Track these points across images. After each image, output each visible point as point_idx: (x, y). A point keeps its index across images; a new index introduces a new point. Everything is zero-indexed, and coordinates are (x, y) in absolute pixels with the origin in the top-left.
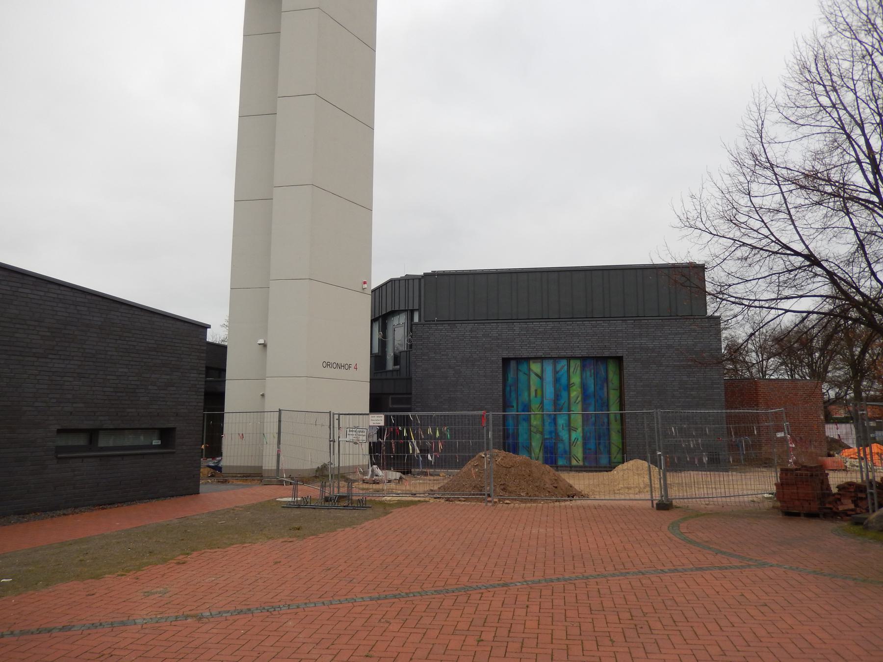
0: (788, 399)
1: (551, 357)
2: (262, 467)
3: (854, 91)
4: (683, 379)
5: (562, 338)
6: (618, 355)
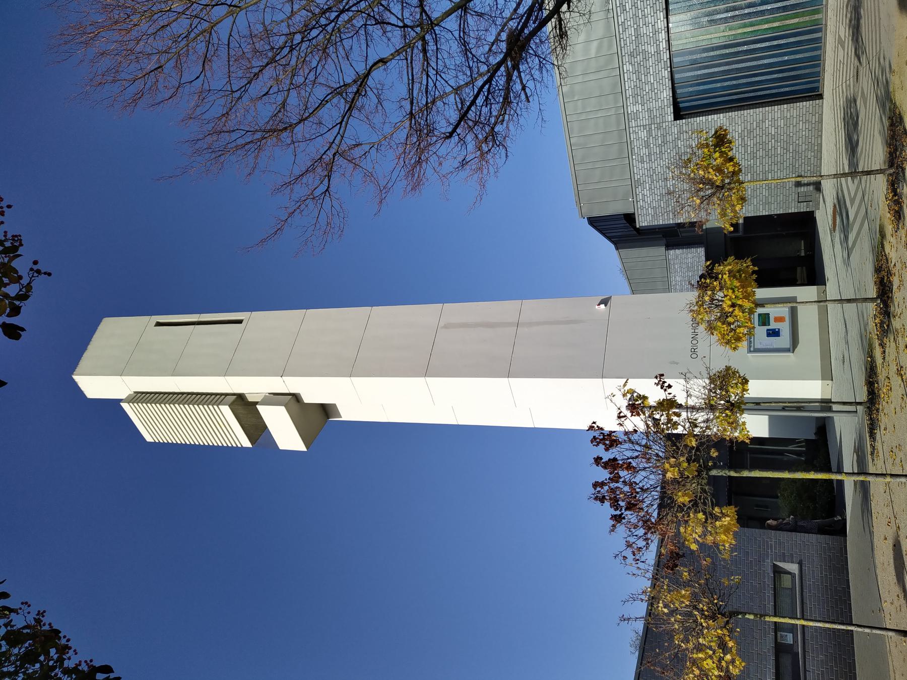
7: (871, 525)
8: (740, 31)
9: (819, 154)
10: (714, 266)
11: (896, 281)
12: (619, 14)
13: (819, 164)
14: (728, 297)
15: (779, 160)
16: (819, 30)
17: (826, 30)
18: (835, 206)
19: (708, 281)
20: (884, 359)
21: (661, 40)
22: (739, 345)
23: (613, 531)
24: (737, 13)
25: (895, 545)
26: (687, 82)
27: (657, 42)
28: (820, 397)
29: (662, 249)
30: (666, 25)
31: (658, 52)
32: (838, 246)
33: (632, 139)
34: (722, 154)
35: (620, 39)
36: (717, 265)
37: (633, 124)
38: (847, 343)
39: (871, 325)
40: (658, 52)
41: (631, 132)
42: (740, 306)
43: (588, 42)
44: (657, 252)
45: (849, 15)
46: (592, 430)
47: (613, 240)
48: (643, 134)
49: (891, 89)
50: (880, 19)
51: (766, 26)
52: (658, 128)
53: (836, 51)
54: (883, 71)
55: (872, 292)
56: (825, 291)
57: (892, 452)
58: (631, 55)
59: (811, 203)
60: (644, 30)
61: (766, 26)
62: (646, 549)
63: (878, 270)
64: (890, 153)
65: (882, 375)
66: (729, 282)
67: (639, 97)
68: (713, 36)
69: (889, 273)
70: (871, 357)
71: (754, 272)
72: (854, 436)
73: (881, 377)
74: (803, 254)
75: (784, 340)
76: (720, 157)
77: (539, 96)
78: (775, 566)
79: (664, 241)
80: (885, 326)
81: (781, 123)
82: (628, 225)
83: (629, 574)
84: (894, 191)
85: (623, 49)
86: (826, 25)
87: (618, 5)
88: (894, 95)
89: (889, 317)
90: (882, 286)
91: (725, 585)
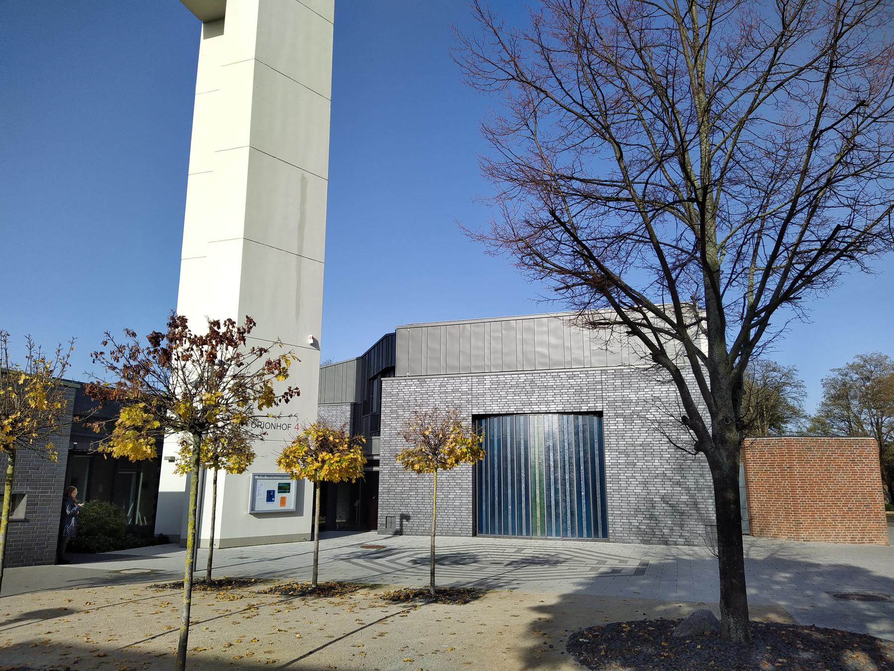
0: (832, 460)
1: (788, 80)
2: (180, 535)
3: (746, 240)
4: (622, 419)
5: (621, 474)
6: (597, 410)
7: (79, 587)
8: (537, 471)
9: (464, 535)
10: (360, 445)
11: (337, 599)
12: (567, 373)
13: (418, 533)
14: (332, 457)
15: (426, 501)
16: (528, 533)
17: (527, 539)
18: (384, 547)
19: (347, 440)
20: (259, 593)
21: (540, 407)
22: (282, 466)
23: (128, 333)
24: (552, 469)
25: (66, 609)
26: (502, 427)
27: (539, 403)
28: (202, 538)
29: (352, 400)
30: (551, 411)
31: (531, 404)
32: (350, 550)
33: (462, 378)
34: (464, 454)
35: (547, 373)
36: (361, 448)
37: (475, 380)
38: (260, 560)
39: (287, 581)
40: (531, 404)
41: (468, 378)
42: (322, 467)
43: (549, 345)
44: (350, 394)
45: (541, 556)
46: (247, 321)
47: (367, 356)
48: (464, 388)
49: (497, 590)
50: (547, 580)
51: (538, 492)
52: (467, 401)
53: (511, 546)
54: (509, 583)
55: (321, 580)
56: (306, 540)
57: (168, 604)
58: (532, 381)
59: (385, 527)
60: (550, 393)
61: (538, 492)
62: (109, 367)
63: (341, 584)
64: (445, 591)
65: (244, 591)
66: (346, 458)
67: (496, 386)
68: (537, 449)
69: (342, 594)
70: (256, 582)
71: (350, 480)
72: (169, 570)
73: (239, 592)
74: (337, 521)
75: (263, 505)
76: (462, 453)
77: (561, 300)
78: (22, 496)
79: (359, 402)
80: (292, 592)
81: (457, 503)
82: (381, 370)
83: (60, 345)
84: (416, 595)
85: (538, 375)
86: (531, 539)
87: (574, 373)
88: (493, 592)
89: (301, 595)
90: (328, 588)
91: (46, 446)
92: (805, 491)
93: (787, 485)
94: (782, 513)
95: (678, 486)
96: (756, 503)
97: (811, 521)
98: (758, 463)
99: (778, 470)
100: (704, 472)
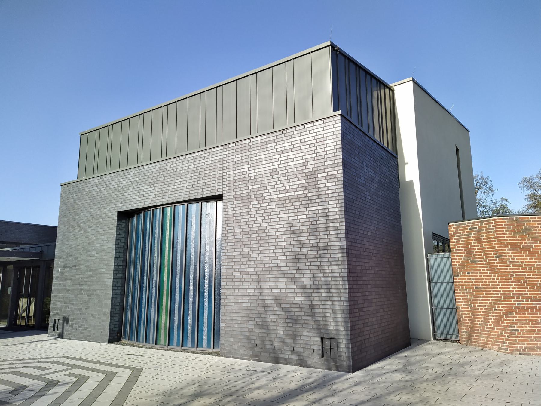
92: (522, 288)
93: (497, 279)
94: (492, 316)
95: (293, 283)
96: (462, 302)
97: (531, 327)
98: (464, 253)
99: (485, 261)
100: (322, 264)
